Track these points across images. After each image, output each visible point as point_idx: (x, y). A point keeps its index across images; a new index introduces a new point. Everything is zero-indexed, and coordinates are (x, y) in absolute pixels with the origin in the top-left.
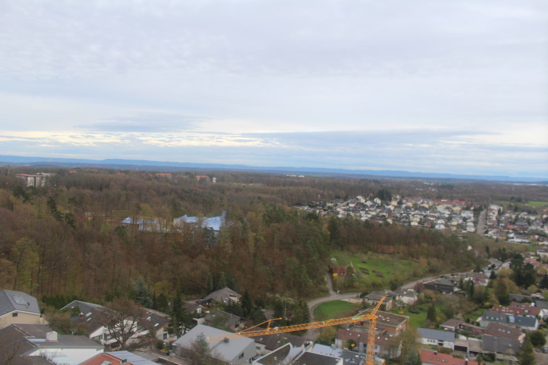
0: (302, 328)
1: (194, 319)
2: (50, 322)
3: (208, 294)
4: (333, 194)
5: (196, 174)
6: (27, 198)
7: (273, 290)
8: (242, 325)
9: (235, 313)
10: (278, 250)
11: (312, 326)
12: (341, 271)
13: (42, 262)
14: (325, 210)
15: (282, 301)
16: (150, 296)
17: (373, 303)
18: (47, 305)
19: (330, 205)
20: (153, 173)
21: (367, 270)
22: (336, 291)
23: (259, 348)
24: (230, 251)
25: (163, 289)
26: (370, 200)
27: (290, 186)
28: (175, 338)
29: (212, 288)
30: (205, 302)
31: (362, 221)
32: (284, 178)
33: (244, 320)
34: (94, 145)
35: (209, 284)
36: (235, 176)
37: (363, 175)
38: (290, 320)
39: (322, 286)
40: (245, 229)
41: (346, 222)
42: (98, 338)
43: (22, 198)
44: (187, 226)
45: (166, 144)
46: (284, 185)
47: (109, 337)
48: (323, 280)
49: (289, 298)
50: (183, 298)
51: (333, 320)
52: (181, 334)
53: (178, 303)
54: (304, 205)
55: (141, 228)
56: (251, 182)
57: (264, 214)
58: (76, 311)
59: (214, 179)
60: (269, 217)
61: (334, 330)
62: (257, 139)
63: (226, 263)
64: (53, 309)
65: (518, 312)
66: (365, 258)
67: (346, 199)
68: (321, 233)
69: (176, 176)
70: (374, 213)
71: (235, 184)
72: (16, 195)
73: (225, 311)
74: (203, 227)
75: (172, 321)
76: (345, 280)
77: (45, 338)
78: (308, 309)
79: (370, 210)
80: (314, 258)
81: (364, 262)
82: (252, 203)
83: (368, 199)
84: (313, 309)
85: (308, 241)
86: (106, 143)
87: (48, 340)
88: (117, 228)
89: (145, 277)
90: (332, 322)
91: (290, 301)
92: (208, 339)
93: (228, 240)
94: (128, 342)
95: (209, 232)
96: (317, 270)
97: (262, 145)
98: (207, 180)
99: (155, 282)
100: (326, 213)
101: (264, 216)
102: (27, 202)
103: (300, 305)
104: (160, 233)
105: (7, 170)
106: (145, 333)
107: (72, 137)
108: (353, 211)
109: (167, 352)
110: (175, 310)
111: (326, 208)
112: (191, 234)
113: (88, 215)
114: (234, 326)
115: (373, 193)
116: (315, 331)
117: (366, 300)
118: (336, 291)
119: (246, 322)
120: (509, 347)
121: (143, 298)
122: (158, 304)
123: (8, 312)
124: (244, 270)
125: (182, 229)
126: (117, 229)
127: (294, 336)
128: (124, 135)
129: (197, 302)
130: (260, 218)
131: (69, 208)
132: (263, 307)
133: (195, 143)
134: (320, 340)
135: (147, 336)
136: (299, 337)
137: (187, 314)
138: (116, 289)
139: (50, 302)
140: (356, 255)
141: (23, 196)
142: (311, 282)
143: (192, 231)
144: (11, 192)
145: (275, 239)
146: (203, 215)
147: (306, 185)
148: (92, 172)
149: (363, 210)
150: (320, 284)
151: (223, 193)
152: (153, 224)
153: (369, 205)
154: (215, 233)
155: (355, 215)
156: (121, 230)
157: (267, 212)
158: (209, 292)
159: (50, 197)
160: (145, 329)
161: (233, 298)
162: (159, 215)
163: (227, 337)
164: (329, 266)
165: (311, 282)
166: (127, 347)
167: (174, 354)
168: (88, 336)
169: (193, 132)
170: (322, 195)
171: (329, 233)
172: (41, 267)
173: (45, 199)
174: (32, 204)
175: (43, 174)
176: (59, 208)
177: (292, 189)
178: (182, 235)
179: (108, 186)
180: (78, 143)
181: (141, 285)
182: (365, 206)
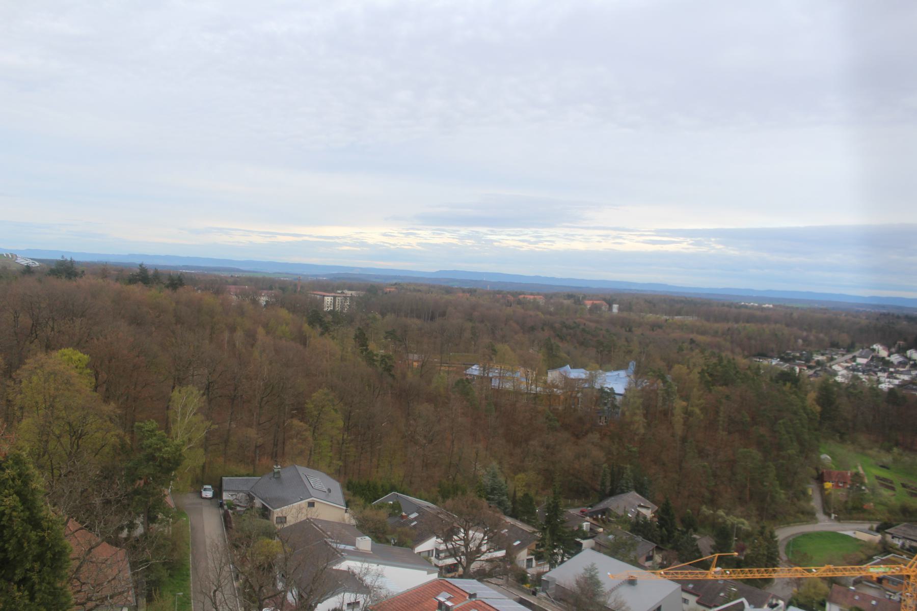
0: (766, 576)
1: (578, 540)
2: (359, 521)
3: (601, 500)
4: (827, 339)
5: (584, 297)
7: (713, 503)
8: (658, 558)
9: (646, 537)
10: (725, 433)
11: (782, 573)
12: (840, 480)
13: (347, 429)
14: (810, 367)
15: (728, 522)
17: (903, 545)
18: (354, 495)
19: (820, 358)
20: (515, 294)
21: (892, 482)
22: (829, 515)
23: (685, 601)
24: (642, 431)
25: (528, 485)
26: (898, 352)
27: (748, 322)
28: (546, 567)
29: (608, 491)
30: (597, 513)
31: (881, 390)
32: (736, 307)
33: (662, 549)
34: (419, 248)
35: (603, 484)
36: (650, 302)
37: (884, 307)
38: (743, 558)
39: (803, 503)
40: (668, 393)
41: (851, 390)
43: (319, 329)
44: (569, 383)
45: (532, 247)
46: (737, 321)
47: (442, 555)
48: (804, 493)
49: (742, 520)
50: (562, 502)
51: (832, 567)
52: (556, 562)
53: (554, 511)
54: (772, 357)
55: (495, 383)
56: (679, 314)
57: (703, 370)
58: (396, 509)
59: (615, 307)
60: (711, 375)
61: (824, 587)
62: (681, 239)
63: (634, 449)
64: (362, 501)
65: (124, 534)
66: (887, 459)
67: (850, 348)
68: (804, 408)
69: (552, 301)
70: (906, 378)
71: (651, 317)
72: (311, 323)
73: (631, 531)
74: (597, 386)
75: (543, 539)
76: (848, 496)
77: (354, 545)
78: (776, 541)
79: (897, 372)
80: (789, 451)
81: (884, 467)
82: (681, 349)
83: (893, 350)
84: (785, 543)
85: (781, 421)
86: (436, 245)
88: (458, 382)
89: (500, 463)
90: (830, 570)
91: (743, 524)
92: (601, 577)
93: (638, 411)
94: (475, 566)
95: (606, 395)
96: (795, 473)
97: (693, 249)
98: (603, 308)
99: (516, 474)
100: (811, 372)
101: (702, 372)
102: (326, 335)
103: (762, 533)
105: (296, 285)
106: (501, 553)
107: (384, 235)
108: (863, 372)
109: (532, 589)
110: (548, 521)
111: (812, 364)
112: (575, 397)
113: (415, 360)
114: (644, 558)
115: (905, 340)
116: (788, 583)
117: (889, 537)
118: (829, 515)
119: (665, 553)
121: (496, 497)
122: (521, 509)
123: (302, 500)
124: (664, 464)
125: (562, 389)
127: (747, 587)
128: (464, 231)
129: (582, 512)
130: (695, 376)
131: (385, 347)
132: (695, 530)
133: (579, 245)
134: (797, 600)
135: (502, 559)
136: (758, 591)
137: (567, 530)
138: (454, 479)
139: (360, 491)
140: (870, 452)
141: (321, 325)
142: (782, 495)
143: (578, 392)
144: (305, 318)
145: (721, 414)
146: (598, 366)
147: (776, 322)
148: (419, 291)
149: (884, 371)
150: (799, 500)
151: (630, 330)
152: (514, 378)
153: (895, 362)
154: (618, 397)
155: (869, 380)
156: (464, 386)
157: (708, 366)
158: (604, 496)
159: (359, 329)
160: (500, 549)
161: (643, 511)
162: (526, 363)
163: (635, 575)
164: (817, 469)
165: (782, 495)
167: (544, 594)
168: (413, 548)
169: (574, 227)
170: (805, 340)
171: (818, 408)
172: (345, 436)
173: (352, 332)
174: (333, 338)
175: (346, 291)
176: (372, 346)
177: (751, 327)
178: (562, 397)
179: (443, 314)
180: (394, 245)
181: (494, 476)
182: (886, 364)
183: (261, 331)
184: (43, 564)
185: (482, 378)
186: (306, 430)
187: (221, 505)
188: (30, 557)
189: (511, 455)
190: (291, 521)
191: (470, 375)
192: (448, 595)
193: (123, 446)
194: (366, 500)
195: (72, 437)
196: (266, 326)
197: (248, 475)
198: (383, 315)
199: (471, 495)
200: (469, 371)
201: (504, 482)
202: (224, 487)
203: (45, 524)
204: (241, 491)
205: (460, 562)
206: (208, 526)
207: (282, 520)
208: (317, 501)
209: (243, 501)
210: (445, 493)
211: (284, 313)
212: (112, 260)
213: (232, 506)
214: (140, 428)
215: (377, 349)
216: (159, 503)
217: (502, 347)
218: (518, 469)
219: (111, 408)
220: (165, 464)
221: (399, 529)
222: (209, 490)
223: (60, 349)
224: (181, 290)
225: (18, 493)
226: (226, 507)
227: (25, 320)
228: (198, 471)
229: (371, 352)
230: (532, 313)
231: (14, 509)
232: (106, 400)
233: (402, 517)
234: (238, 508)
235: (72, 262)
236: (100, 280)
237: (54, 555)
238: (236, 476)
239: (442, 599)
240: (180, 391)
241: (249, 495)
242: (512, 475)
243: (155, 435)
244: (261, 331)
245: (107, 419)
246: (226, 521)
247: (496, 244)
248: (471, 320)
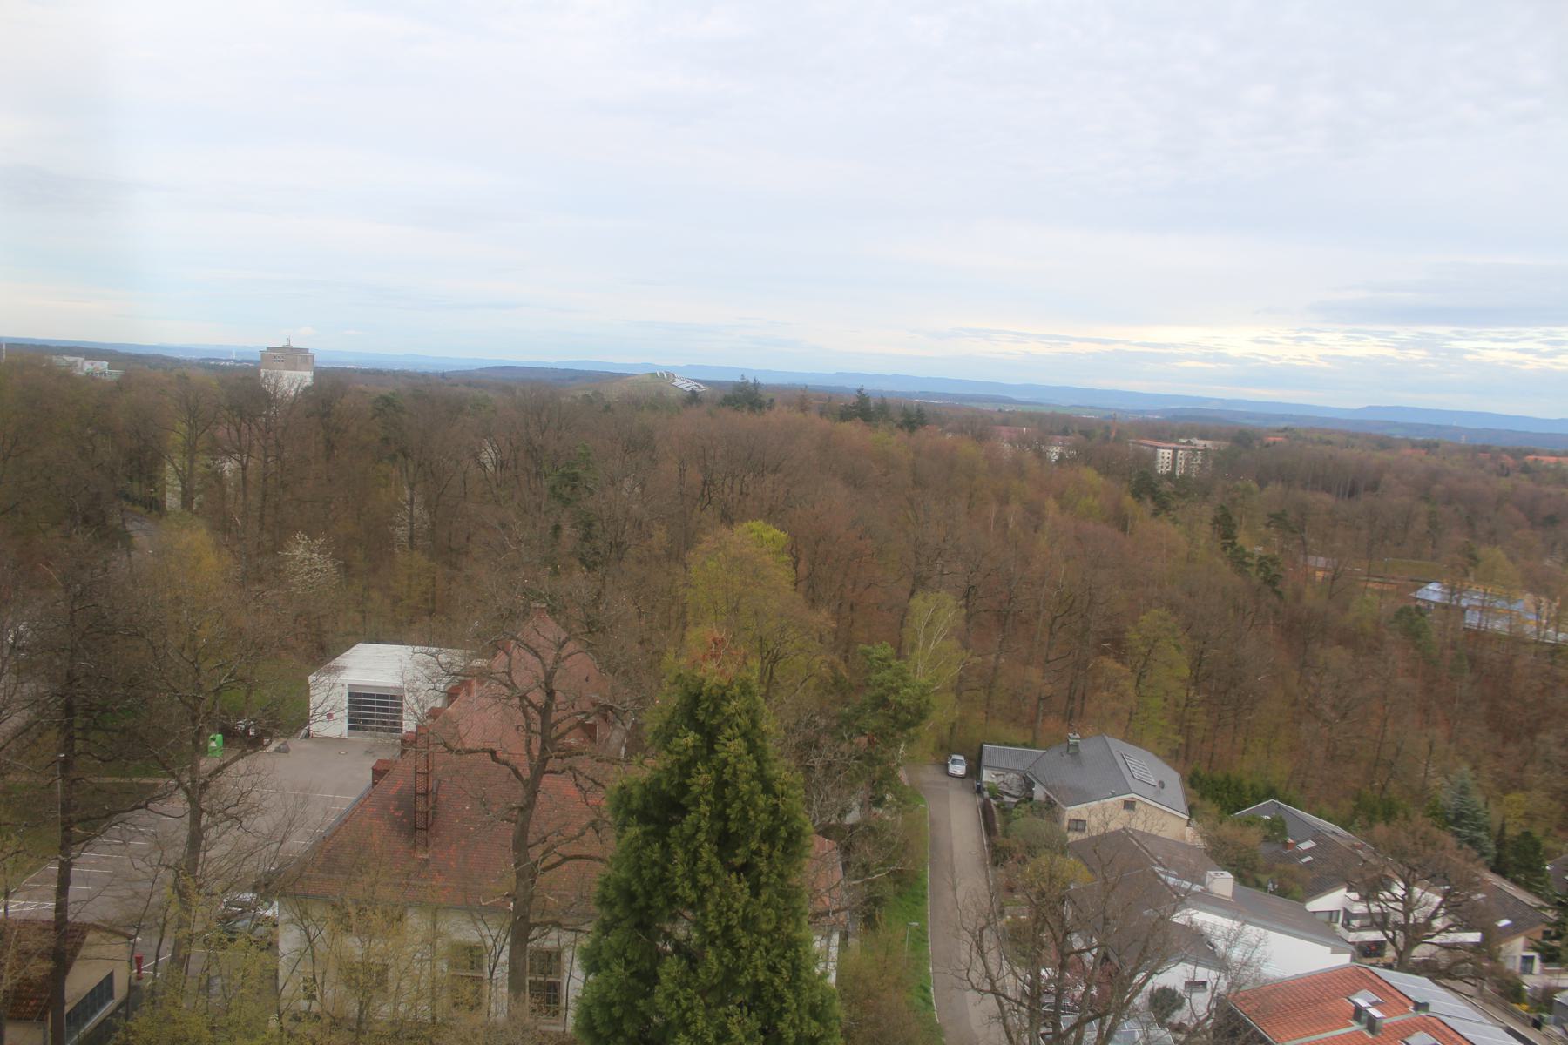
6: (1162, 506)
13: (1196, 680)
16: (1488, 829)
18: (1202, 796)
20: (1518, 453)
34: (1324, 364)
42: (1325, 917)
43: (1150, 505)
45: (1545, 363)
47: (1355, 923)
55: (1472, 619)
58: (1277, 830)
64: (1215, 809)
72: (1136, 494)
87: (1207, 890)
88: (1401, 611)
94: (1420, 952)
99: (1505, 792)
102: (1163, 514)
104: (1536, 642)
105: (1107, 428)
106: (1474, 937)
107: (1257, 341)
109: (1533, 1015)
120: (1089, 987)
121: (1465, 831)
122: (1518, 859)
123: (1114, 795)
126: (1400, 614)
128: (1405, 333)
131: (1265, 542)
135: (1476, 947)
138: (1384, 788)
139: (1214, 792)
141: (1154, 499)
144: (1125, 485)
148: (1329, 442)
156: (1411, 619)
160: (1470, 929)
166: (1417, 964)
167: (1557, 1031)
168: (1304, 901)
173: (1208, 511)
174: (1175, 522)
175: (1195, 441)
176: (1242, 539)
179: (1374, 487)
180: (1277, 358)
181: (1464, 791)
183: (1051, 505)
184: (773, 846)
185: (1446, 607)
186: (1126, 678)
187: (979, 790)
188: (758, 833)
189: (1499, 755)
190: (1095, 824)
191: (1424, 601)
192: (1374, 998)
193: (837, 681)
194: (1222, 809)
195: (763, 659)
196: (1059, 497)
197: (1025, 745)
198: (1262, 484)
199: (1420, 822)
200: (1421, 594)
201: (1482, 805)
202: (986, 760)
203: (778, 787)
204: (1013, 771)
205: (1393, 941)
206: (957, 824)
207: (1078, 825)
208: (1135, 797)
209: (1014, 786)
210: (1368, 810)
211: (1090, 475)
212: (811, 382)
213: (996, 793)
214: (866, 654)
215: (1251, 544)
216: (888, 778)
217: (1493, 554)
218: (1510, 785)
219: (822, 618)
220: (902, 716)
221: (1280, 867)
222: (960, 762)
223: (742, 520)
224: (921, 432)
225: (744, 735)
226: (986, 794)
227: (694, 476)
228: (946, 731)
229: (1241, 549)
230: (1550, 489)
231: (738, 757)
232: (814, 603)
233: (1286, 845)
234: (1006, 799)
235: (756, 385)
236: (800, 415)
237: (790, 835)
238: (1006, 744)
239: (1363, 1003)
240: (925, 599)
241: (1025, 778)
242: (1497, 793)
243: (889, 666)
244: (1051, 505)
245: (816, 636)
246: (986, 814)
247: (1468, 357)
248: (1426, 499)
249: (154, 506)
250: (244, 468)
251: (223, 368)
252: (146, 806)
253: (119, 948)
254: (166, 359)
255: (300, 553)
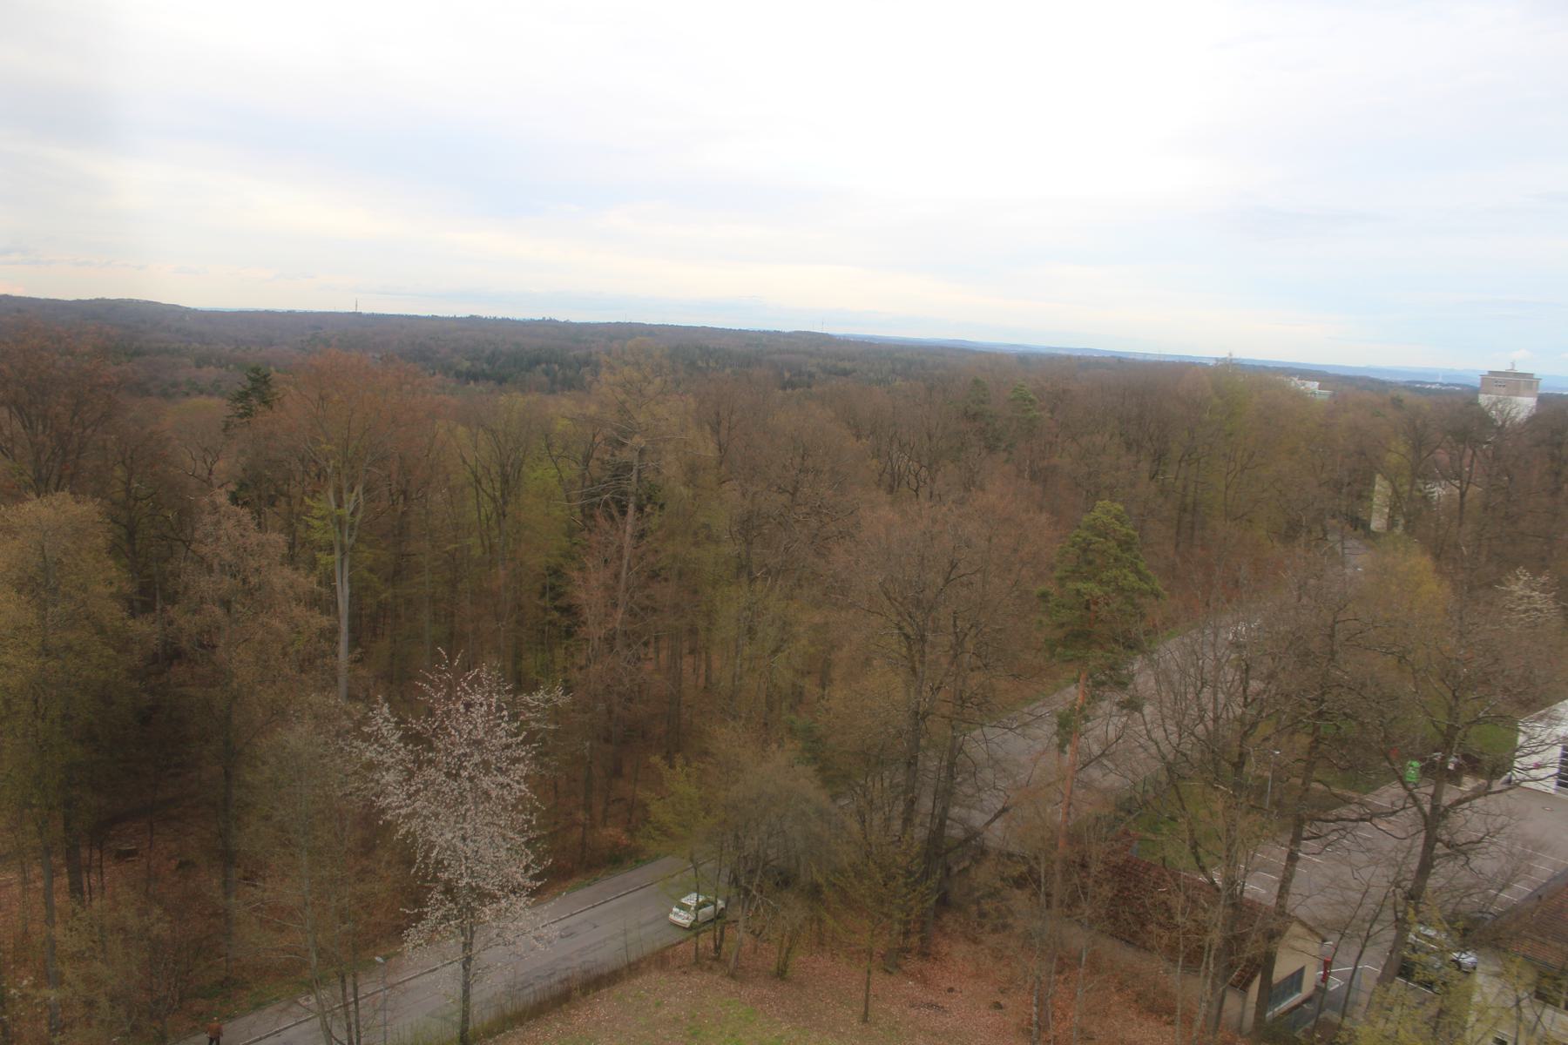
249: (1359, 524)
250: (1462, 495)
251: (1430, 391)
252: (1370, 820)
253: (1313, 946)
254: (1372, 380)
255: (1517, 588)
